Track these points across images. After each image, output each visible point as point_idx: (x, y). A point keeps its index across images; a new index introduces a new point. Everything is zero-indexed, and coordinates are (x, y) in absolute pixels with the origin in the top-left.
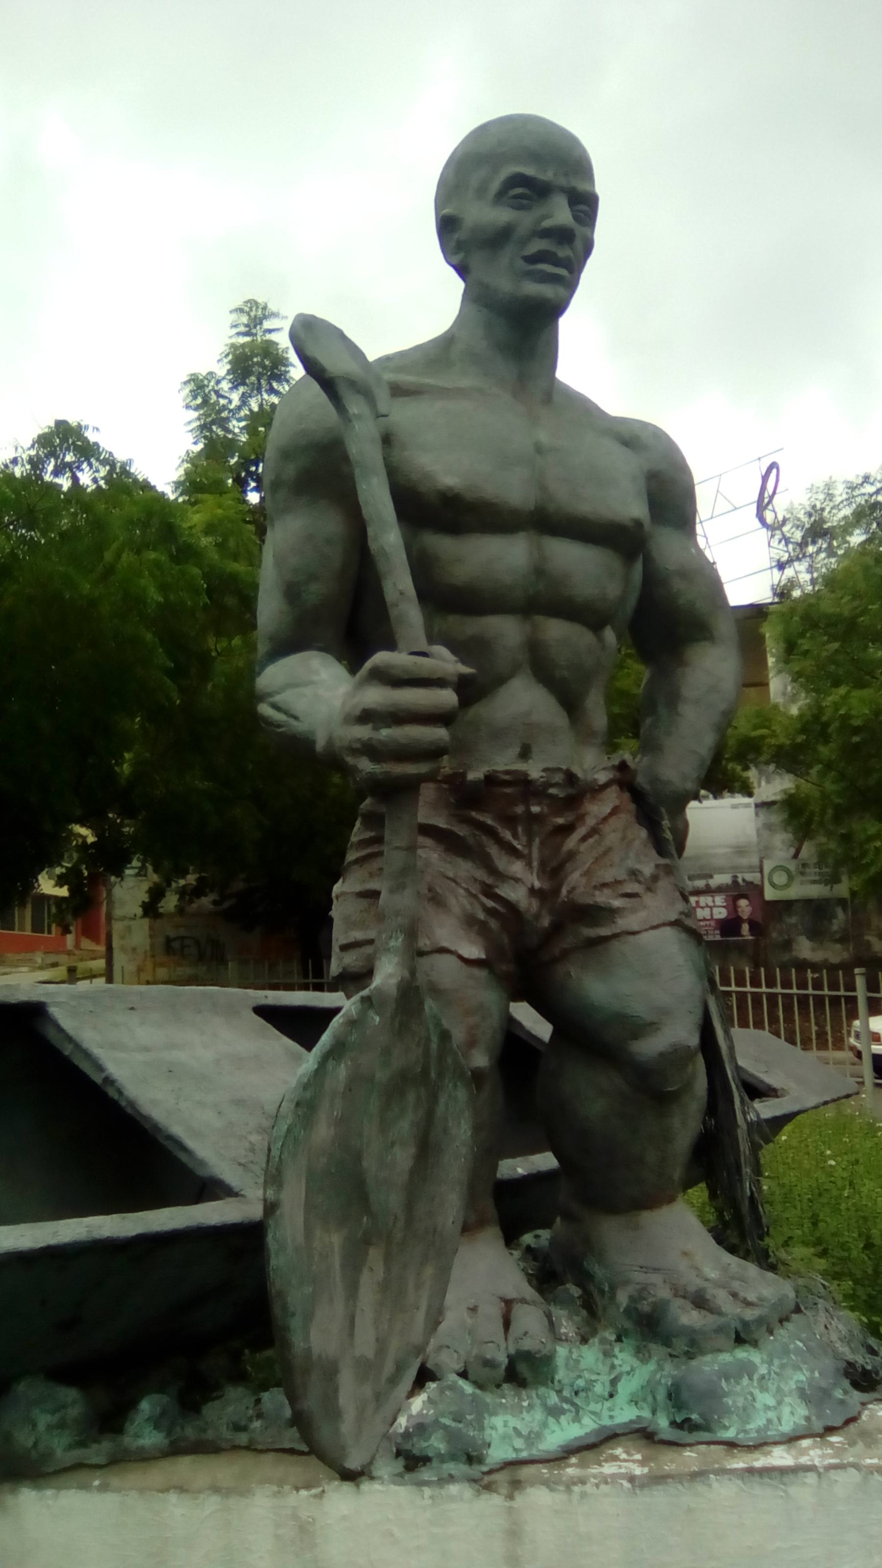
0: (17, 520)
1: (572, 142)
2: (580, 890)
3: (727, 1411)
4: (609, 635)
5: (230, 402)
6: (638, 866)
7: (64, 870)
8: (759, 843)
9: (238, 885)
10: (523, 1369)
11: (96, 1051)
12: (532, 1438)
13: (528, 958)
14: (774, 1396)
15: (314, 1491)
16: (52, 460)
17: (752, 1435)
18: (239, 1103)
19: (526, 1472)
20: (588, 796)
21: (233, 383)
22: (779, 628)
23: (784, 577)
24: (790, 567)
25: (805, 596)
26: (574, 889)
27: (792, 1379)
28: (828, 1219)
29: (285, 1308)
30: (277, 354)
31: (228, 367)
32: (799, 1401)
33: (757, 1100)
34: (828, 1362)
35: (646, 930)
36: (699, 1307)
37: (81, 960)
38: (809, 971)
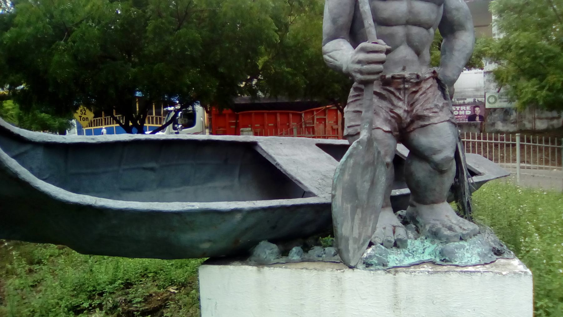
10: (398, 243)
11: (273, 156)
12: (400, 261)
18: (314, 171)
29: (336, 222)
34: (487, 247)
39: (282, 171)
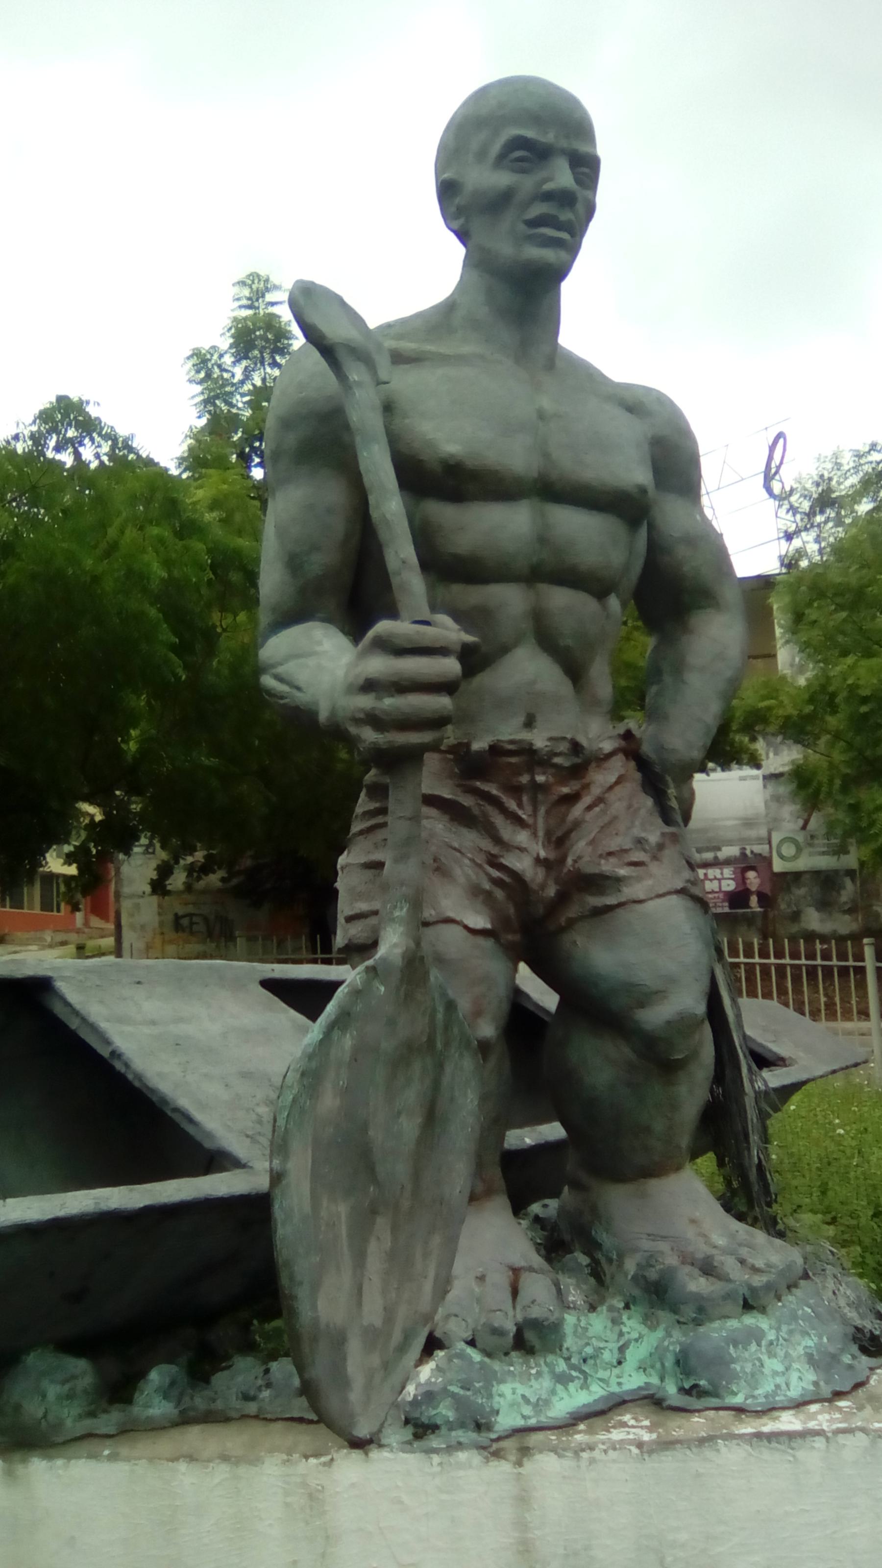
0: (21, 497)
1: (573, 103)
2: (587, 859)
3: (735, 1377)
4: (614, 602)
5: (233, 376)
6: (643, 835)
7: (72, 849)
8: (767, 815)
9: (247, 862)
10: (530, 1336)
11: (103, 1025)
12: (540, 1405)
13: (534, 926)
14: (782, 1362)
15: (323, 1459)
16: (55, 437)
17: (760, 1401)
18: (246, 1075)
19: (535, 1438)
20: (593, 765)
21: (236, 357)
22: (787, 599)
23: (791, 548)
24: (797, 537)
25: (813, 566)
26: (580, 858)
27: (799, 1344)
28: (837, 1188)
29: (292, 1278)
30: (280, 327)
31: (231, 341)
32: (807, 1366)
33: (765, 1070)
34: (836, 1328)
35: (651, 899)
36: (707, 1274)
37: (91, 938)
38: (818, 941)
39: (130, 1077)
